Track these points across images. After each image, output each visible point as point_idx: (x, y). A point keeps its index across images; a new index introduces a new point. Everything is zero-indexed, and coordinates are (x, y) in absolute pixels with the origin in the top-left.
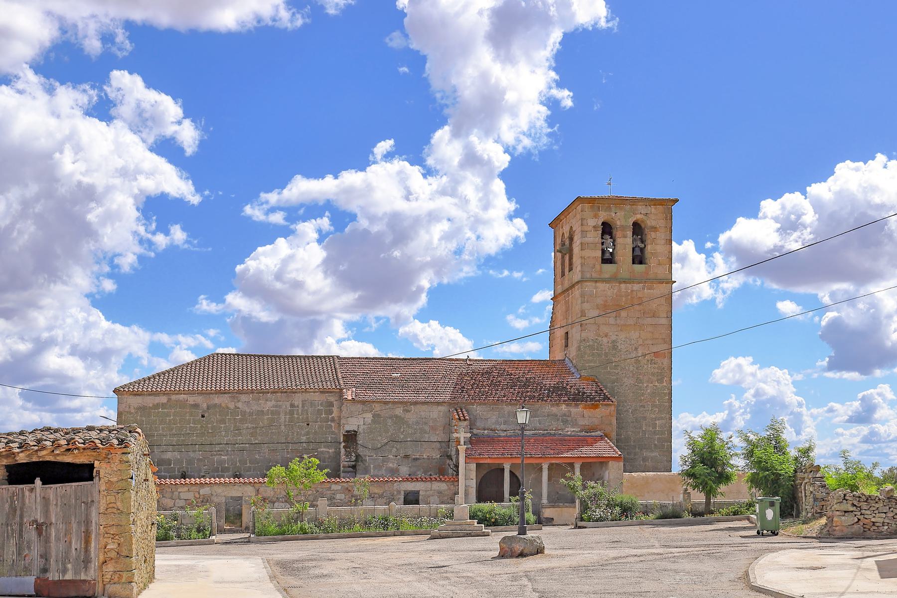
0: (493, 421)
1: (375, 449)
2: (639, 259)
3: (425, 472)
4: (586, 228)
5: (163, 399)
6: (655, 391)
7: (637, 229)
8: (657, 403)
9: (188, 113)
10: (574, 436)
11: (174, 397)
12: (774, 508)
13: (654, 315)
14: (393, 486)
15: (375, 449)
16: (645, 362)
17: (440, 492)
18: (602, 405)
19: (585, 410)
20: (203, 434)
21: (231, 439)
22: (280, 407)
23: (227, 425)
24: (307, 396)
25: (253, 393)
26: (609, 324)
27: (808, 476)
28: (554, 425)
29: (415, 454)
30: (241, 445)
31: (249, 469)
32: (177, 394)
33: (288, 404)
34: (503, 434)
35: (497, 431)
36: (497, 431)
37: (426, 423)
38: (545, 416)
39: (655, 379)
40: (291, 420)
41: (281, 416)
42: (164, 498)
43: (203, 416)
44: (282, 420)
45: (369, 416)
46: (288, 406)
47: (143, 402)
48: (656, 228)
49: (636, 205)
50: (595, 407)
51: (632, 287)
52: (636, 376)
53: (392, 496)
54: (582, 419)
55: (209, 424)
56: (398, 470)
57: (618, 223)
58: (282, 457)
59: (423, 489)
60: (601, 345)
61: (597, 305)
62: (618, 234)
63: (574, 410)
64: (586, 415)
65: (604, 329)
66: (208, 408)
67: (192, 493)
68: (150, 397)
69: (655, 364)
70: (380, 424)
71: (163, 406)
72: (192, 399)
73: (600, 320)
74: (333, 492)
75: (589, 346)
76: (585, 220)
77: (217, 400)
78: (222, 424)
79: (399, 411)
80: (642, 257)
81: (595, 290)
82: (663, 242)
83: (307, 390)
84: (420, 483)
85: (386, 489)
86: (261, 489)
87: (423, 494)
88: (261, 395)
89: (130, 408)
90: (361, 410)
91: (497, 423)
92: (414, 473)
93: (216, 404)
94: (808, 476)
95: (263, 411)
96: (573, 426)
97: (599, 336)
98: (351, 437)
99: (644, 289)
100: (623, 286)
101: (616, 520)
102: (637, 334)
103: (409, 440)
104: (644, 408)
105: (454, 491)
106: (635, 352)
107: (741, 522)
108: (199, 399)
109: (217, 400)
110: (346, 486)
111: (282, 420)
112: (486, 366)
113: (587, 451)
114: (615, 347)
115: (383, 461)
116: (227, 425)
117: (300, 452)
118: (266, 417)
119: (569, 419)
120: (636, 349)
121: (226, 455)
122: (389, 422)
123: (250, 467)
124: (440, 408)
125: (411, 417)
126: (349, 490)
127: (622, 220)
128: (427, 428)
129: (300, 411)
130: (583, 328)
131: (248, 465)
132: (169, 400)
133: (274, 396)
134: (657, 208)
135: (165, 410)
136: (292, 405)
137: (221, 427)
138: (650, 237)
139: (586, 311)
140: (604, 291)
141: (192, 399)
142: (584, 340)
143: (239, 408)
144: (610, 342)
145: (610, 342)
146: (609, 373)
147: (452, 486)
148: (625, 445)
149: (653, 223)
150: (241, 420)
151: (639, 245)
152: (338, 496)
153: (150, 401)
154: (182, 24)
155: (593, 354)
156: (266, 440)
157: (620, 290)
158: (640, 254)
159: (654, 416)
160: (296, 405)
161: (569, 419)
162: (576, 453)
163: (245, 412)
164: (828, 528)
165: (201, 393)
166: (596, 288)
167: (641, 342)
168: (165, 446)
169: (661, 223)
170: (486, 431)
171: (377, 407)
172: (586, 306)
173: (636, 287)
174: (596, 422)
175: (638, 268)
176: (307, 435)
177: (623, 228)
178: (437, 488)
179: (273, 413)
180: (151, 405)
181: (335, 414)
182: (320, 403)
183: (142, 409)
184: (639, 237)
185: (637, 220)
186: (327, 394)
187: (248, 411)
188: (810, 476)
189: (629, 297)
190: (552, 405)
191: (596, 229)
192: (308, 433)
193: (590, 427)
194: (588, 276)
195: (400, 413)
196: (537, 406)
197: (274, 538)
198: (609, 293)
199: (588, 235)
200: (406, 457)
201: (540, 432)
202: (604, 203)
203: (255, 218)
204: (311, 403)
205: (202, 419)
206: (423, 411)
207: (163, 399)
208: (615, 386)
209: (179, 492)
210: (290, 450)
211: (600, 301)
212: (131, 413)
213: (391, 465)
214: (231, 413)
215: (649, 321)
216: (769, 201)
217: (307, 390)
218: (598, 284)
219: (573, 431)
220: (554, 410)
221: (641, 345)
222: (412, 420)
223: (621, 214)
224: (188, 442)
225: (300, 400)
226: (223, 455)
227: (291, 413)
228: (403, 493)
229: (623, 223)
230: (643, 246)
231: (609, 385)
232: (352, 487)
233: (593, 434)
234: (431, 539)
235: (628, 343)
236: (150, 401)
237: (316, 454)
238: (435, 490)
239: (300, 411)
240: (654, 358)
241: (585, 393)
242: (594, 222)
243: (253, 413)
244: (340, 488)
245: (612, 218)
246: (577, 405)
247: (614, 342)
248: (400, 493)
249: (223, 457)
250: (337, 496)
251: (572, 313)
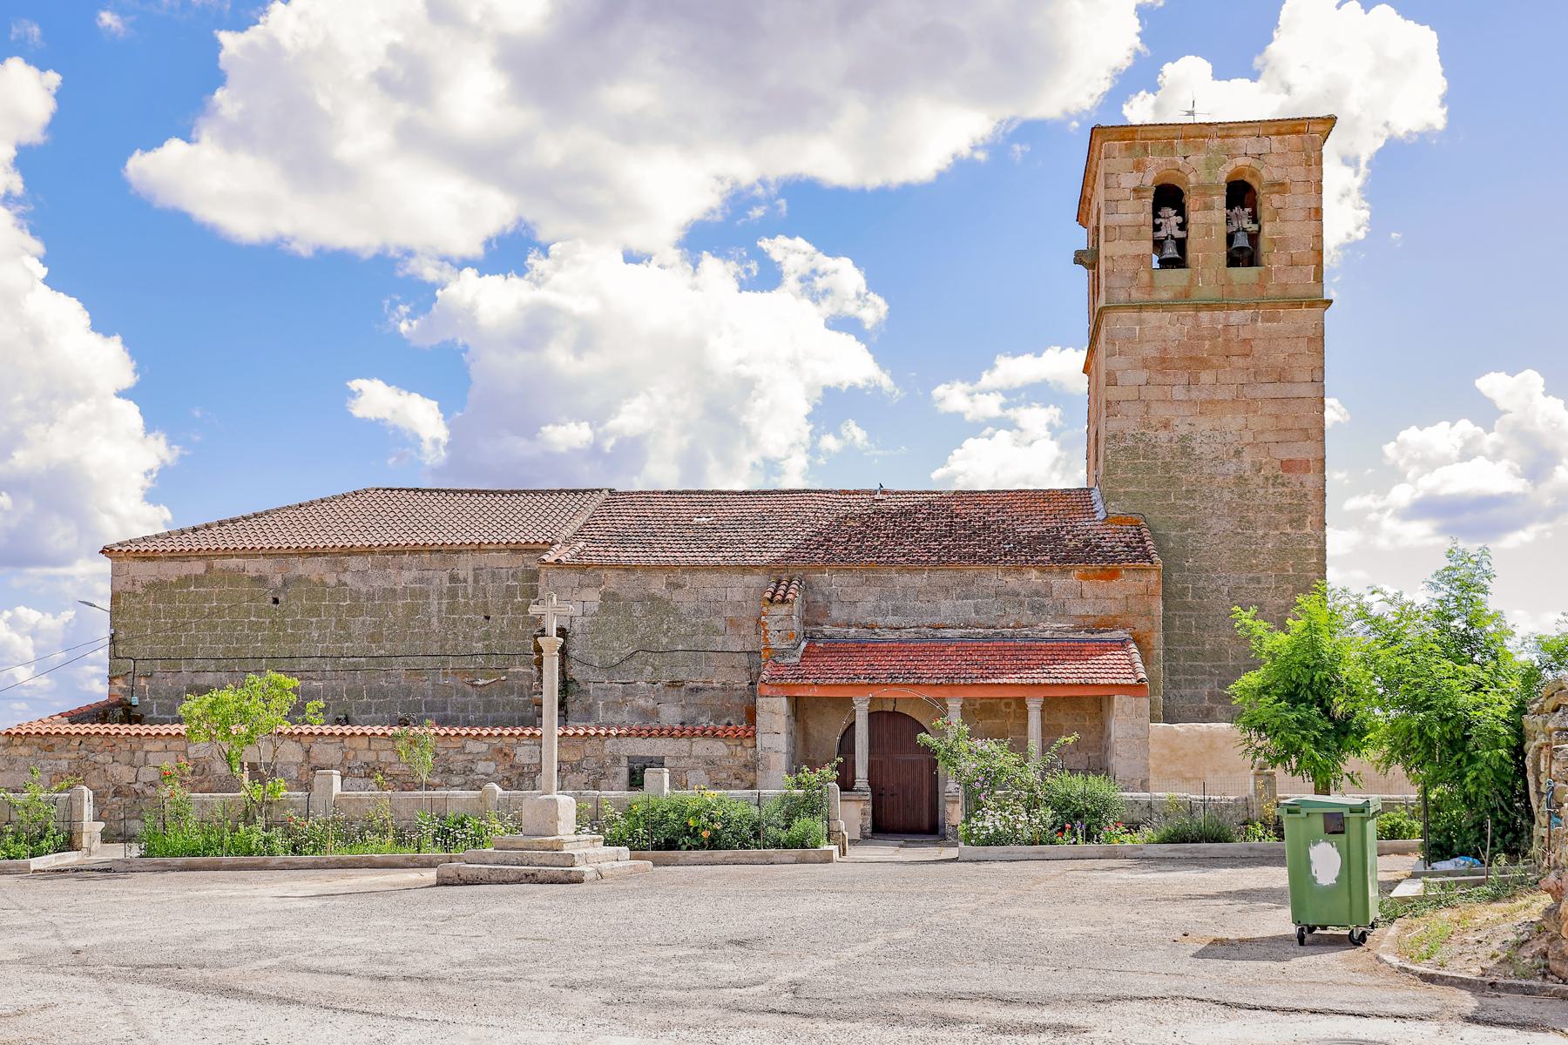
0: (869, 607)
1: (608, 668)
2: (1243, 255)
3: (717, 718)
4: (1115, 194)
5: (198, 568)
6: (1283, 546)
7: (1240, 193)
8: (1291, 572)
9: (873, 285)
10: (1057, 640)
11: (218, 563)
12: (1343, 838)
13: (1281, 377)
14: (603, 744)
15: (608, 668)
16: (1260, 481)
17: (711, 762)
18: (1127, 570)
19: (1085, 583)
20: (276, 639)
21: (331, 646)
22: (429, 581)
23: (323, 618)
24: (483, 559)
25: (372, 553)
26: (1172, 401)
27: (1545, 723)
28: (1013, 615)
29: (694, 679)
30: (351, 659)
31: (366, 709)
32: (224, 556)
33: (445, 576)
34: (890, 635)
35: (877, 630)
36: (877, 630)
37: (716, 613)
38: (988, 596)
39: (1284, 518)
40: (452, 609)
41: (431, 600)
42: (115, 764)
43: (276, 601)
44: (434, 608)
45: (593, 597)
46: (446, 579)
47: (159, 572)
48: (1283, 184)
49: (1232, 137)
50: (1114, 575)
51: (1227, 318)
52: (1237, 513)
53: (602, 767)
54: (1079, 601)
55: (288, 616)
56: (658, 713)
57: (1192, 178)
58: (433, 685)
59: (672, 753)
60: (1154, 447)
61: (1144, 360)
62: (1191, 202)
63: (1057, 582)
64: (1088, 592)
66: (285, 583)
67: (173, 754)
68: (173, 564)
69: (1283, 485)
70: (618, 613)
71: (199, 580)
72: (252, 567)
73: (1152, 393)
74: (470, 757)
75: (1125, 449)
76: (1114, 176)
77: (302, 568)
78: (313, 617)
79: (658, 585)
80: (1253, 253)
81: (1138, 328)
82: (1303, 214)
83: (483, 547)
84: (663, 741)
85: (588, 752)
86: (315, 749)
87: (671, 765)
88: (390, 557)
89: (134, 584)
90: (576, 585)
91: (877, 610)
92: (693, 721)
93: (301, 576)
94: (1545, 723)
95: (395, 590)
96: (1055, 619)
97: (1149, 426)
99: (1254, 320)
100: (1205, 316)
101: (1041, 843)
102: (1240, 420)
103: (680, 647)
104: (1259, 583)
105: (742, 760)
106: (1234, 460)
107: (1405, 857)
108: (265, 566)
109: (302, 568)
110: (499, 745)
111: (434, 608)
112: (907, 504)
113: (1069, 673)
114: (1186, 451)
115: (625, 694)
116: (323, 618)
117: (470, 675)
118: (400, 603)
119: (1048, 601)
120: (1238, 453)
121: (321, 680)
122: (638, 610)
123: (369, 705)
124: (748, 578)
125: (685, 600)
126: (505, 754)
128: (719, 623)
129: (470, 590)
130: (1110, 410)
131: (365, 700)
132: (209, 568)
133: (415, 560)
134: (1284, 140)
135: (202, 589)
136: (453, 579)
137: (312, 623)
138: (1268, 205)
139: (1118, 374)
140: (1160, 327)
141: (252, 567)
142: (1114, 437)
143: (345, 584)
144: (1176, 439)
145: (1176, 439)
146: (1173, 507)
147: (739, 748)
148: (1213, 666)
149: (1277, 175)
150: (350, 609)
151: (1246, 226)
152: (481, 767)
153: (172, 571)
154: (874, 181)
155: (1135, 468)
156: (402, 648)
157: (1197, 326)
158: (1248, 245)
159: (1283, 602)
160: (461, 577)
161: (1048, 601)
162: (1027, 677)
163: (358, 592)
164: (1541, 944)
165: (269, 554)
166: (1140, 322)
167: (1248, 437)
168: (201, 661)
170: (853, 630)
171: (612, 581)
172: (1118, 362)
173: (1236, 317)
174: (1113, 608)
175: (1243, 275)
176: (485, 640)
177: (1204, 189)
178: (705, 753)
179: (413, 594)
180: (174, 580)
182: (510, 573)
183: (157, 586)
184: (1248, 210)
185: (1239, 171)
186: (525, 555)
187: (364, 590)
188: (1551, 725)
189: (1220, 339)
190: (1007, 572)
191: (1140, 195)
192: (487, 636)
193: (1098, 620)
194: (1122, 296)
195: (660, 590)
196: (970, 573)
197: (165, 864)
198: (1172, 332)
199: (1121, 208)
200: (674, 684)
201: (977, 631)
202: (1158, 136)
204: (493, 574)
205: (274, 606)
206: (710, 584)
207: (198, 568)
208: (1188, 535)
209: (147, 752)
210: (450, 671)
211: (1150, 351)
212: (135, 595)
213: (641, 702)
214: (331, 594)
215: (1270, 390)
217: (483, 547)
218: (1145, 315)
219: (1058, 629)
220: (1012, 581)
221: (1248, 444)
222: (685, 604)
223: (1197, 159)
224: (246, 654)
225: (470, 567)
226: (315, 680)
227: (453, 594)
228: (624, 762)
229: (1204, 178)
230: (1255, 227)
231: (1174, 533)
232: (511, 747)
233: (1105, 636)
234: (443, 882)
235: (1218, 441)
236: (172, 571)
237: (503, 678)
238: (697, 757)
239: (470, 590)
240: (1281, 472)
241: (1098, 547)
243: (374, 595)
244: (484, 747)
245: (1178, 170)
246: (1064, 572)
247: (1183, 438)
248: (619, 760)
249: (314, 683)
250: (479, 767)
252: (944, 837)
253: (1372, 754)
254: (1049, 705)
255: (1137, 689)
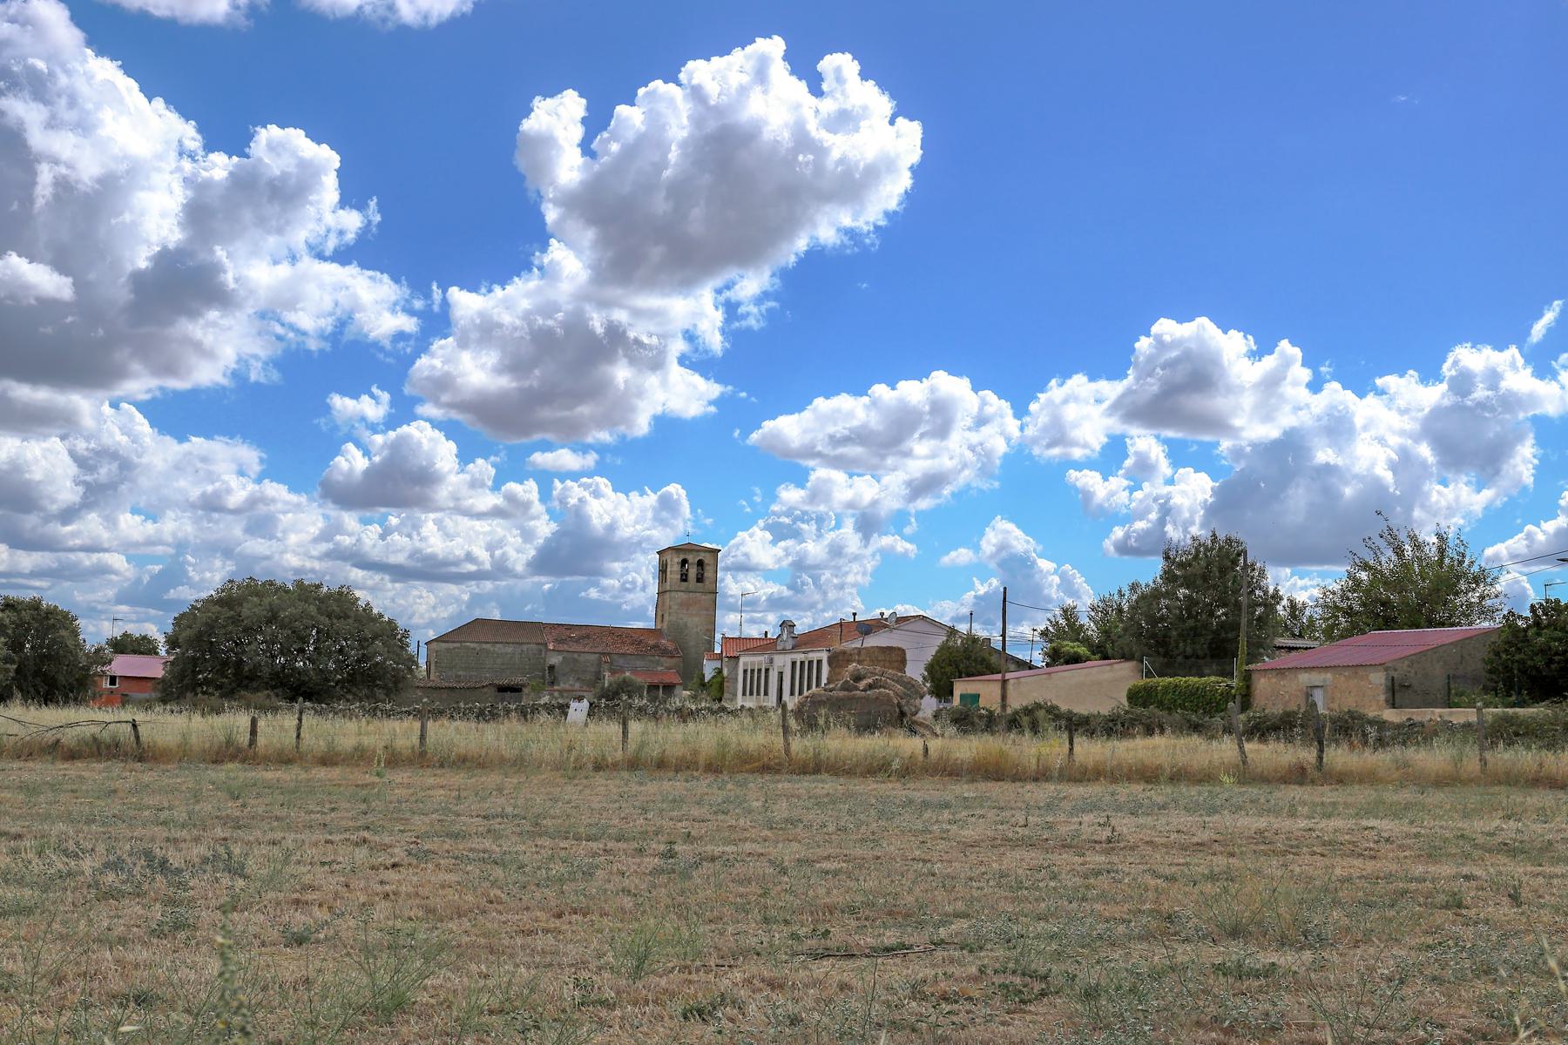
2: (700, 579)
5: (458, 645)
45: (561, 658)
65: (681, 616)
77: (485, 646)
79: (576, 656)
98: (552, 668)
127: (693, 559)
169: (712, 562)
181: (543, 655)
183: (448, 649)
203: (250, 456)
211: (679, 601)
216: (575, 94)
242: (678, 559)
251: (1206, 777)
252: (393, 754)
253: (1112, 390)
254: (664, 687)
255: (680, 684)
